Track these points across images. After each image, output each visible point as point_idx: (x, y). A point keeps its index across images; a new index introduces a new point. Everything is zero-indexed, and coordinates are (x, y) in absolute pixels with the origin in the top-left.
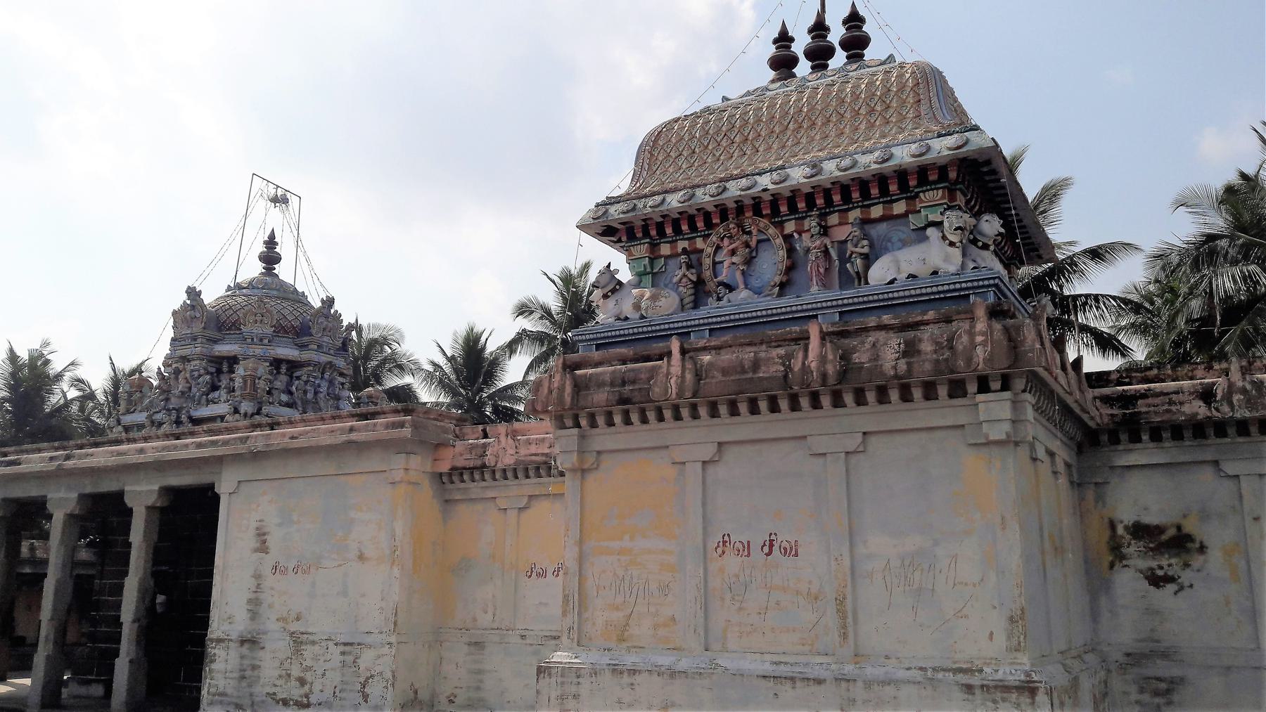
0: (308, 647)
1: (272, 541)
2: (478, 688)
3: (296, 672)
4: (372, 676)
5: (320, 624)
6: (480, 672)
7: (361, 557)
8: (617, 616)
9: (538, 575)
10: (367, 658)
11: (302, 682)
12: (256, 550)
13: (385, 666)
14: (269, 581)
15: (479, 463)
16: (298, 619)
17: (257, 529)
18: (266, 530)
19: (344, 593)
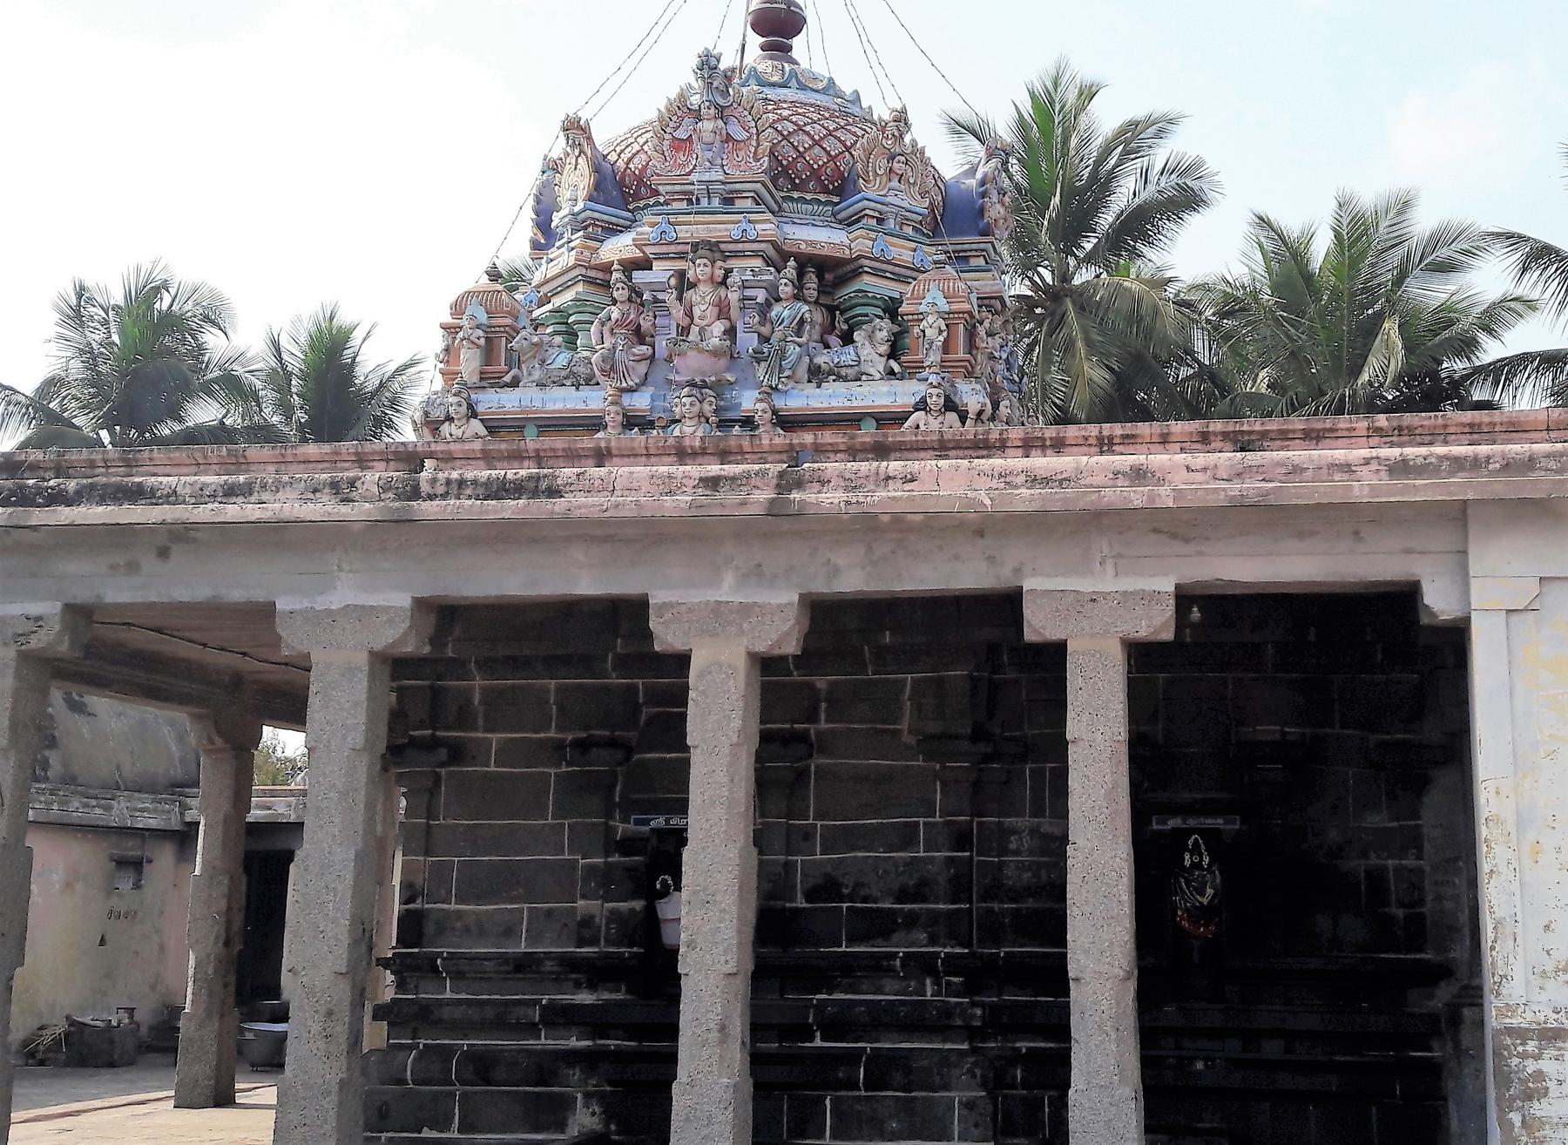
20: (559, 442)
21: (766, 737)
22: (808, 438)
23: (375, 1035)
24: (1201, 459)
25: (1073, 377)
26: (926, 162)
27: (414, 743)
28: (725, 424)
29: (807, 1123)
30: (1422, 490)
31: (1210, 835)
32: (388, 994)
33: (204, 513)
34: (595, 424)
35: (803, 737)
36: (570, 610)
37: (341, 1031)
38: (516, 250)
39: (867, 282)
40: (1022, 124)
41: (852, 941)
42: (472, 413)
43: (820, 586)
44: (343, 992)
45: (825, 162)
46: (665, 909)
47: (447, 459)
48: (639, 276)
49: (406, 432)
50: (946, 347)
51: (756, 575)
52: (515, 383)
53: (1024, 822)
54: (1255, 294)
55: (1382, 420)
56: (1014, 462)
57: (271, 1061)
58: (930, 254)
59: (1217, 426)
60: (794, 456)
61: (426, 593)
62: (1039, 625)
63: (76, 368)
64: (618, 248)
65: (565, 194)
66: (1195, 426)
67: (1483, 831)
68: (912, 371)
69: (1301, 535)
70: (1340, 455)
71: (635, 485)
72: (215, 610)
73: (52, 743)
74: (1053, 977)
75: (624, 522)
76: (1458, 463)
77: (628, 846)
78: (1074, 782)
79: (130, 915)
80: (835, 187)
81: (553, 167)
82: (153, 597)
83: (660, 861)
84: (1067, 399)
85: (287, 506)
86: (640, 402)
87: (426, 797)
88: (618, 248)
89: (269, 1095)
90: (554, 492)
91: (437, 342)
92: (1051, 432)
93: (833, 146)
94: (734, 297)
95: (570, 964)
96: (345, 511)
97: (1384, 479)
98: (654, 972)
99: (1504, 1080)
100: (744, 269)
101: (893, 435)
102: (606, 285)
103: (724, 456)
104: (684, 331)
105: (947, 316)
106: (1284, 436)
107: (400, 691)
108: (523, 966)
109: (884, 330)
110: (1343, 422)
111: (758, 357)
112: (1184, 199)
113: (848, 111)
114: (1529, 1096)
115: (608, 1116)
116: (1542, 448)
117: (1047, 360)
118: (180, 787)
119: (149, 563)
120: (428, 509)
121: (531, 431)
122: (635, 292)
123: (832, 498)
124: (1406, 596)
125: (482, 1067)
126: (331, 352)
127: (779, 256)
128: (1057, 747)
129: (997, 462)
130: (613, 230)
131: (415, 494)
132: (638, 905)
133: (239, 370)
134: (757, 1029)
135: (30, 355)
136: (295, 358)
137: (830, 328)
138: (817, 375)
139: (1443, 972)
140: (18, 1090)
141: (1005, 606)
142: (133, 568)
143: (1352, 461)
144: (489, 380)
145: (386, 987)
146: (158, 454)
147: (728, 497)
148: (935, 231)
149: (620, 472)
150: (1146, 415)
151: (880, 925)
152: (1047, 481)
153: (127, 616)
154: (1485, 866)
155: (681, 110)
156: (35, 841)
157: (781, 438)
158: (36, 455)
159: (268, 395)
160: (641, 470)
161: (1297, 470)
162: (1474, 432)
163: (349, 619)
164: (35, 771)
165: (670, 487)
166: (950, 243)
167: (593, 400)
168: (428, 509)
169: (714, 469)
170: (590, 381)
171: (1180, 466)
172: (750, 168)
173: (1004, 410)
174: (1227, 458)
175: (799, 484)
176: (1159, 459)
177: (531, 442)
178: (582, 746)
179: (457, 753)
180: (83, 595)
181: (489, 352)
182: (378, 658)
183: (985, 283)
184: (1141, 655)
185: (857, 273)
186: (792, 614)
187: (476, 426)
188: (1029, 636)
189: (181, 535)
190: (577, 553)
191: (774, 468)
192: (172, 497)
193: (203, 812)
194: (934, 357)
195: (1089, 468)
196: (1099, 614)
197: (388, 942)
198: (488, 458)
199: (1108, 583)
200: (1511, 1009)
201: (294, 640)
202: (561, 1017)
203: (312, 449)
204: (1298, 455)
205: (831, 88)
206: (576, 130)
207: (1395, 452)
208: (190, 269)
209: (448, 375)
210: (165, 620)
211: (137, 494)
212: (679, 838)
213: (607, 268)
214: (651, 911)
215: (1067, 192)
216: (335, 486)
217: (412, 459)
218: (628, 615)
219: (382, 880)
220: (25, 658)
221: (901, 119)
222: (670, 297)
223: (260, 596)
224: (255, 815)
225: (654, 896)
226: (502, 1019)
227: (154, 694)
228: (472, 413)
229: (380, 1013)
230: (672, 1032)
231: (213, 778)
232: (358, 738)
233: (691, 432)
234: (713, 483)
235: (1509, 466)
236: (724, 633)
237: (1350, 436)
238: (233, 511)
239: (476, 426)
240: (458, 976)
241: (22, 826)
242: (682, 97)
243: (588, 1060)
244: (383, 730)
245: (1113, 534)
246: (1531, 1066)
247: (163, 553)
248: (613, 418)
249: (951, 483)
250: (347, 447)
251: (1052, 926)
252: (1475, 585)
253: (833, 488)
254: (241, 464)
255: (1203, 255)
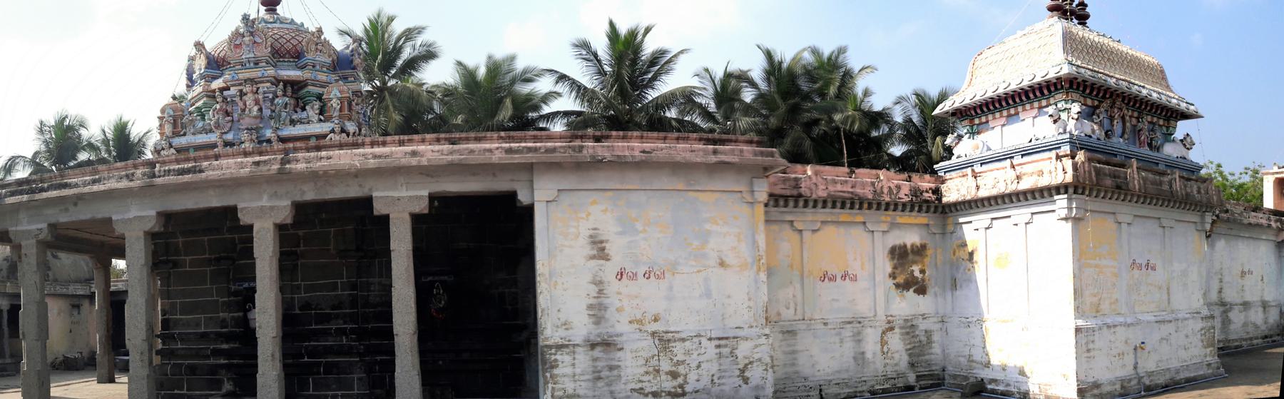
0: (677, 344)
1: (611, 249)
2: (793, 364)
3: (666, 366)
4: (751, 363)
5: (681, 320)
6: (794, 352)
7: (722, 264)
8: (1095, 300)
9: (830, 279)
10: (744, 349)
11: (674, 375)
12: (593, 257)
13: (763, 353)
14: (613, 286)
15: (795, 192)
16: (656, 320)
17: (591, 236)
18: (603, 238)
19: (708, 294)
20: (202, 153)
21: (282, 253)
22: (291, 145)
23: (157, 360)
24: (437, 147)
25: (389, 119)
26: (330, 45)
27: (161, 262)
28: (260, 142)
29: (304, 386)
30: (517, 158)
31: (442, 282)
32: (160, 346)
33: (87, 189)
34: (214, 146)
35: (295, 253)
36: (210, 212)
37: (146, 358)
38: (181, 89)
39: (310, 88)
40: (366, 30)
41: (316, 324)
42: (171, 146)
43: (298, 198)
44: (145, 346)
45: (292, 48)
46: (250, 315)
47: (164, 163)
48: (225, 93)
49: (149, 155)
50: (341, 110)
51: (275, 195)
52: (185, 134)
53: (377, 280)
54: (456, 88)
55: (503, 134)
56: (368, 150)
57: (125, 369)
58: (334, 77)
59: (442, 135)
60: (286, 152)
61: (160, 209)
62: (379, 209)
63: (43, 148)
64: (217, 84)
65: (196, 68)
66: (434, 136)
67: (538, 279)
68: (328, 119)
69: (474, 174)
70: (487, 146)
71: (230, 166)
72: (93, 221)
73: (49, 269)
74: (389, 334)
75: (226, 180)
76: (530, 150)
77: (236, 294)
78: (394, 266)
79: (78, 323)
80: (296, 56)
81: (192, 59)
82: (74, 219)
83: (248, 299)
84: (387, 126)
85: (113, 184)
86: (230, 137)
87: (166, 281)
88: (217, 84)
89: (125, 379)
90: (201, 171)
91: (157, 123)
92: (381, 139)
93: (295, 42)
94: (260, 97)
95: (219, 335)
96: (132, 184)
97: (504, 155)
98: (248, 337)
99: (544, 363)
100: (264, 87)
101: (322, 142)
102: (214, 97)
103: (261, 154)
104: (243, 110)
105: (339, 99)
106: (467, 140)
107: (155, 244)
108: (204, 336)
109: (317, 105)
110: (489, 134)
111: (271, 117)
112: (429, 55)
113: (300, 29)
114: (552, 367)
115: (235, 386)
116: (558, 144)
117: (379, 113)
118: (88, 281)
119: (72, 208)
120: (159, 181)
121: (191, 150)
122: (225, 98)
123: (301, 166)
124: (512, 195)
125: (192, 370)
126: (121, 131)
127: (276, 81)
128: (387, 253)
129: (361, 150)
130: (215, 78)
131: (154, 176)
132: (241, 314)
133: (93, 141)
134: (285, 355)
135: (29, 145)
136: (110, 136)
137: (297, 105)
138: (293, 123)
139: (525, 327)
140: (52, 378)
141: (367, 202)
142: (67, 210)
143: (493, 148)
144: (176, 134)
145: (159, 344)
146: (70, 172)
147: (263, 168)
148: (335, 69)
149: (224, 162)
150: (417, 132)
151: (326, 318)
152: (380, 157)
153: (67, 226)
154: (539, 291)
155: (237, 34)
156: (48, 300)
157: (281, 146)
158: (34, 177)
159: (103, 148)
160: (231, 161)
161: (472, 151)
162: (535, 139)
163: (135, 220)
164: (45, 278)
165: (242, 166)
166: (340, 73)
167: (213, 138)
168: (159, 181)
169: (257, 158)
170: (211, 131)
171: (430, 151)
172: (264, 52)
173: (363, 131)
174: (446, 147)
175: (289, 162)
176: (422, 148)
177: (192, 154)
178: (218, 260)
179: (175, 264)
180: (53, 220)
181: (175, 125)
182: (146, 233)
183: (354, 87)
184: (416, 219)
185: (306, 85)
186: (288, 209)
187: (172, 151)
188: (376, 213)
189: (80, 198)
190: (211, 192)
191: (279, 157)
192: (76, 185)
193: (96, 289)
194: (336, 114)
195: (396, 152)
196: (401, 203)
197: (158, 330)
198: (178, 161)
199: (404, 193)
200: (547, 339)
201: (119, 229)
202: (217, 353)
203: (119, 164)
204: (472, 146)
205: (292, 22)
206: (199, 46)
207: (507, 145)
208: (74, 111)
209: (162, 134)
210: (78, 226)
211: (66, 186)
212: (254, 290)
213: (214, 91)
214: (245, 316)
215: (383, 53)
216: (127, 176)
217: (151, 164)
218: (231, 212)
219: (155, 309)
220: (38, 242)
221: (320, 31)
222: (237, 99)
223: (107, 215)
224: (112, 288)
225: (246, 311)
226: (197, 354)
227: (78, 251)
228: (171, 146)
229: (158, 353)
230: (256, 357)
231: (99, 277)
232: (142, 261)
233: (248, 146)
234: (257, 163)
235: (548, 151)
236: (265, 216)
237: (491, 139)
238: (96, 188)
239: (172, 151)
240: (182, 340)
241: (43, 296)
242: (237, 30)
243: (228, 367)
244: (150, 258)
245: (404, 178)
246: (553, 357)
247: (75, 204)
248: (220, 143)
249: (344, 158)
250: (130, 162)
251: (388, 317)
252: (536, 193)
253: (301, 162)
254: (96, 172)
255: (437, 75)
